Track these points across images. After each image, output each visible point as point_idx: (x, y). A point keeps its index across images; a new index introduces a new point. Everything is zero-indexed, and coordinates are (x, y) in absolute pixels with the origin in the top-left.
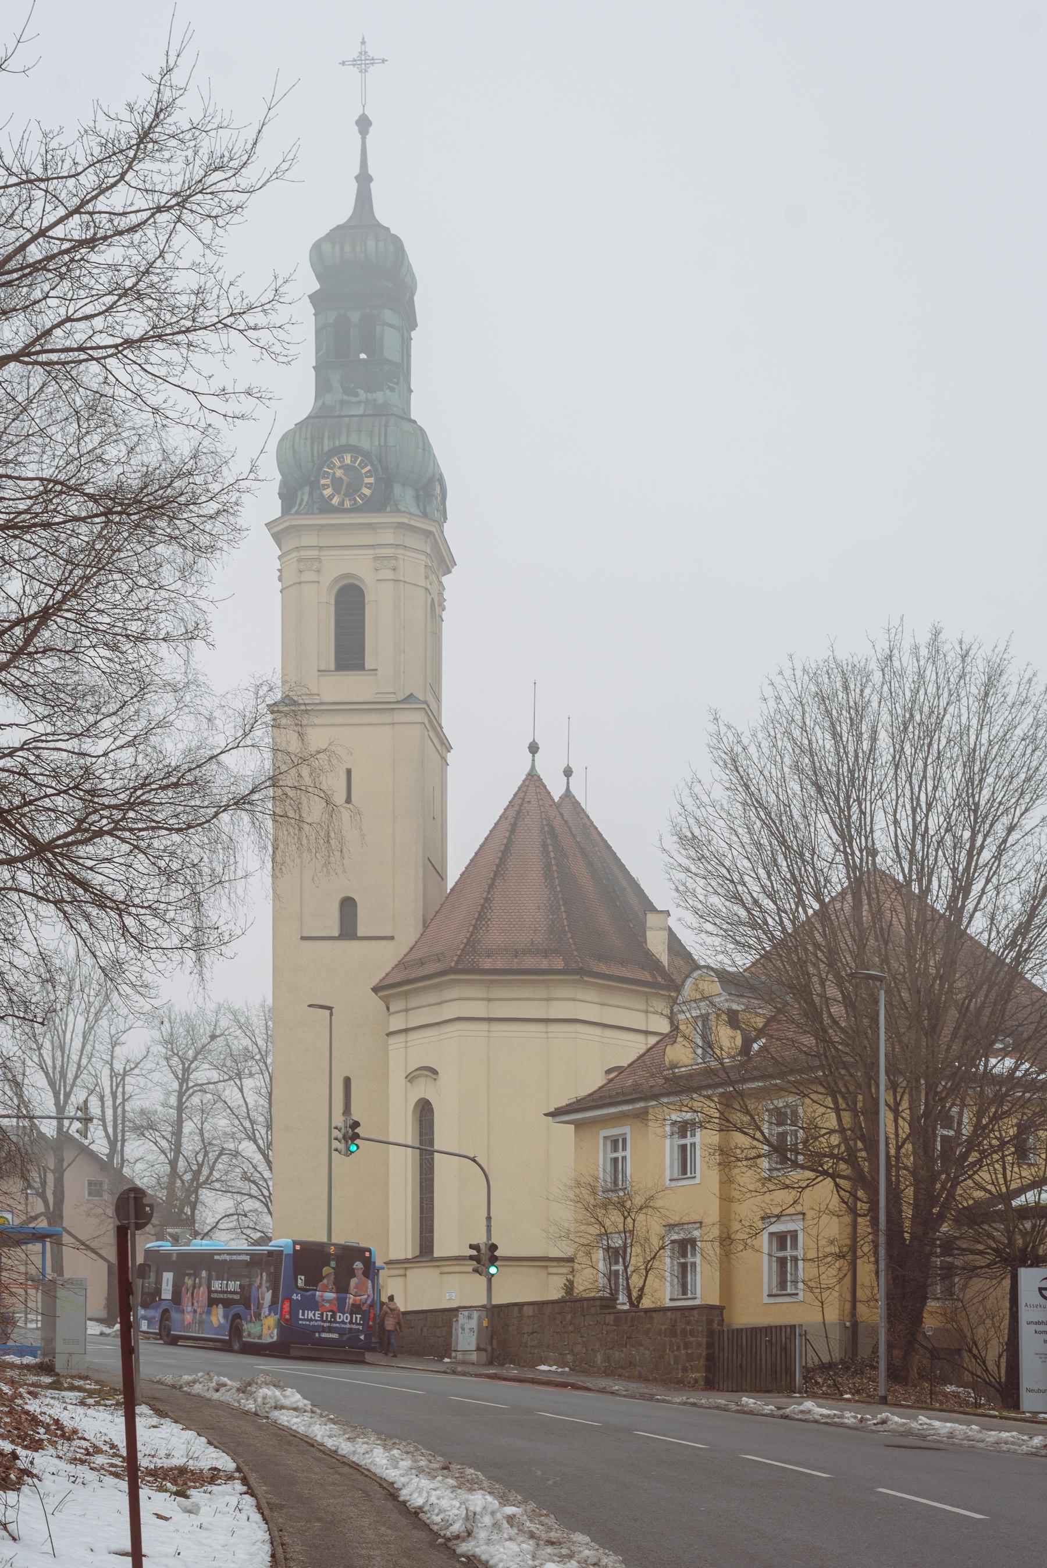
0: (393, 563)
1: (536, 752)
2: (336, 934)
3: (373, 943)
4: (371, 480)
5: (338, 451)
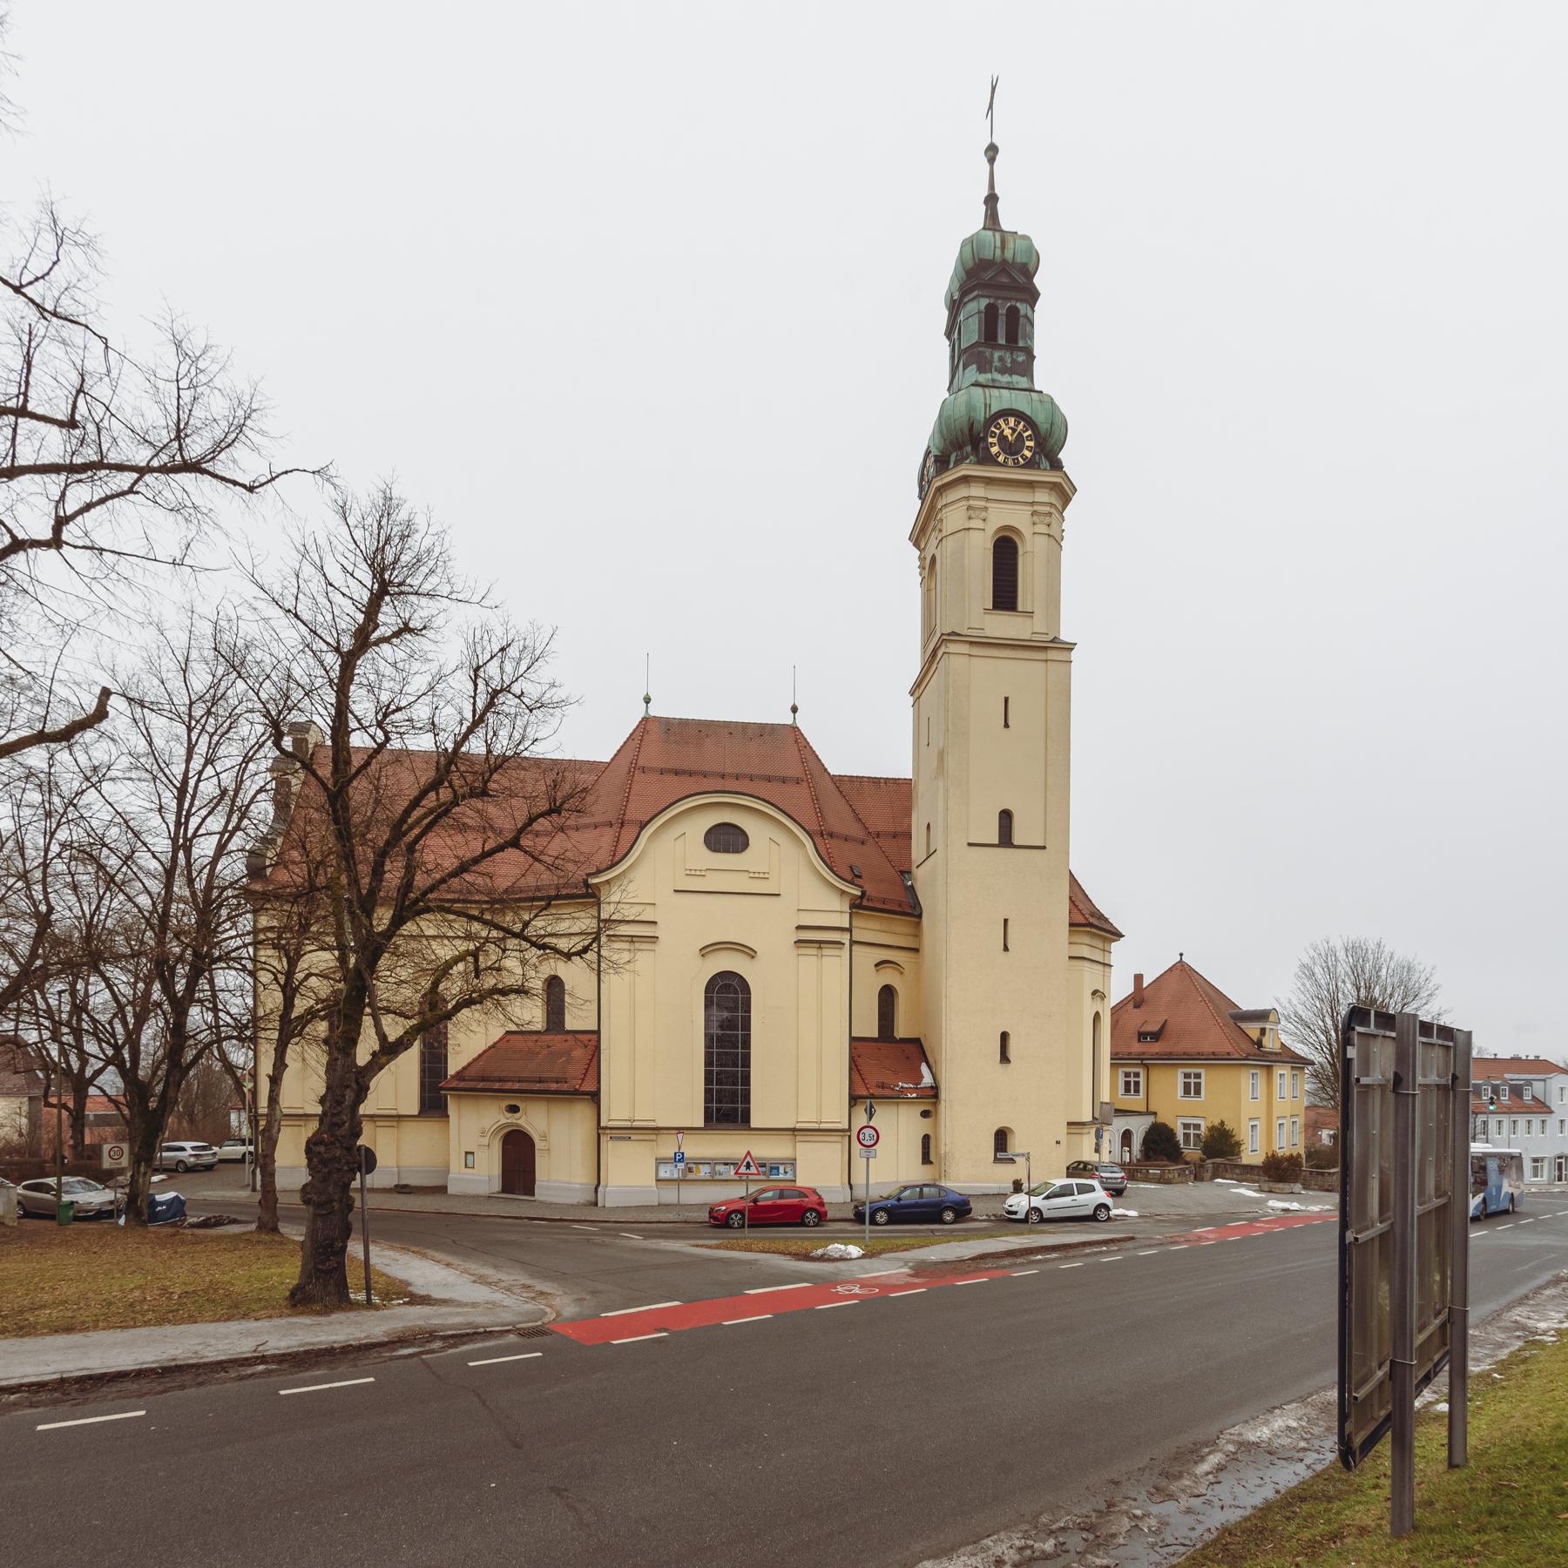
0: (1047, 520)
4: (1031, 444)
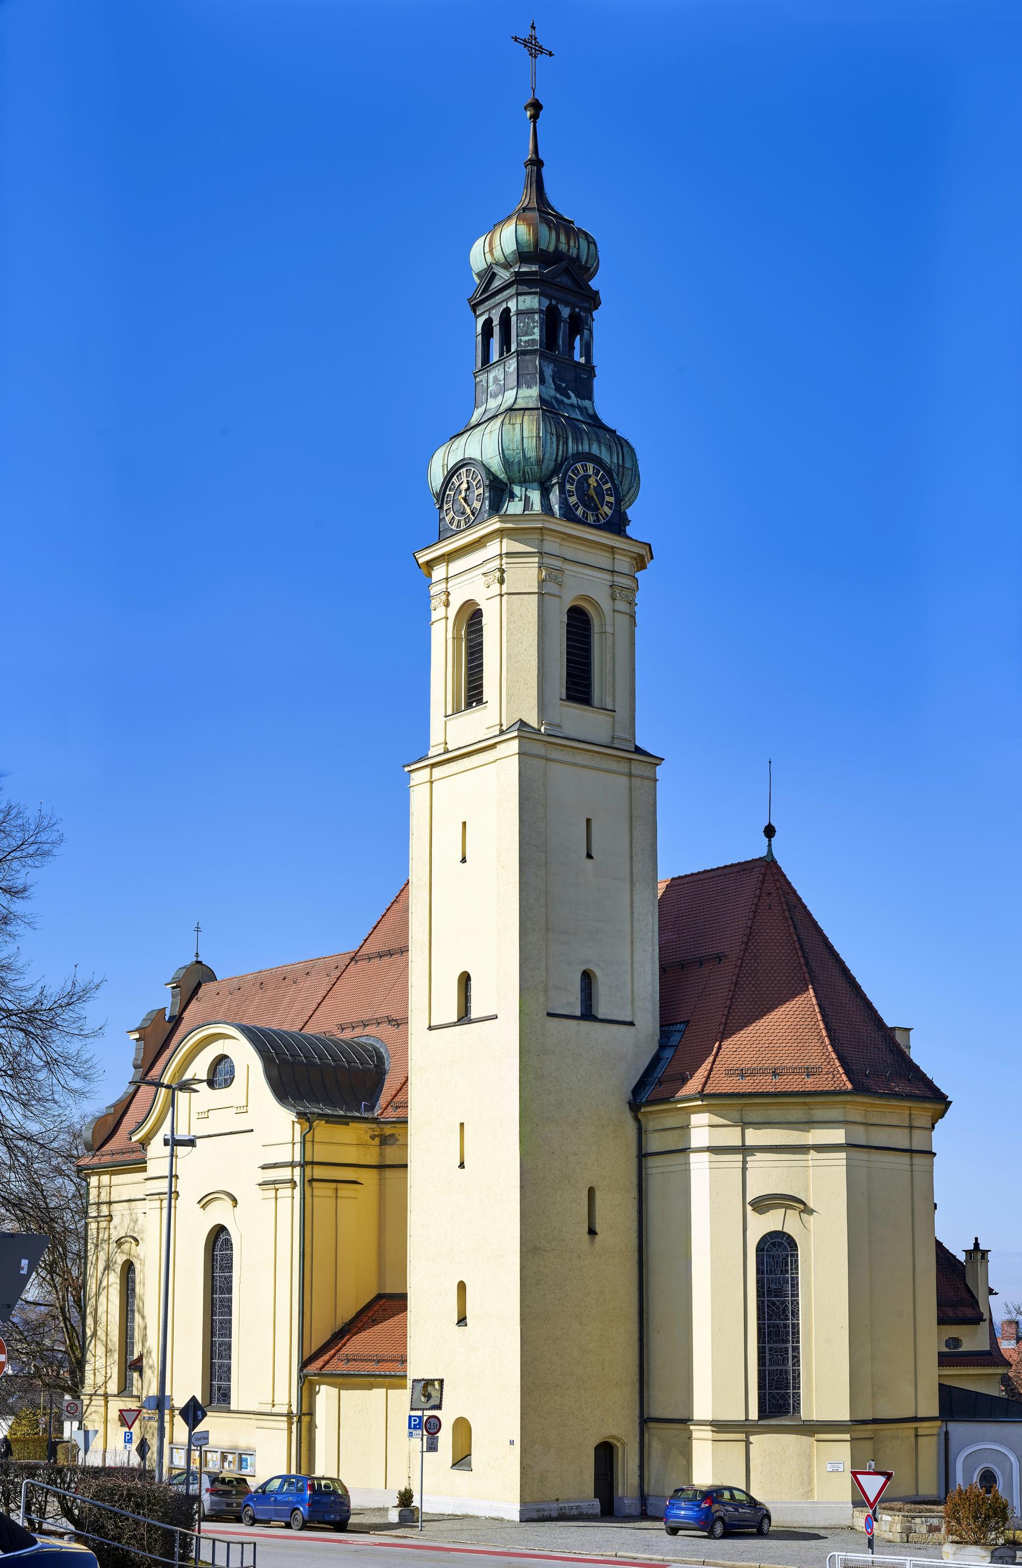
1: (766, 827)
2: (578, 1013)
3: (615, 1027)
5: (579, 457)
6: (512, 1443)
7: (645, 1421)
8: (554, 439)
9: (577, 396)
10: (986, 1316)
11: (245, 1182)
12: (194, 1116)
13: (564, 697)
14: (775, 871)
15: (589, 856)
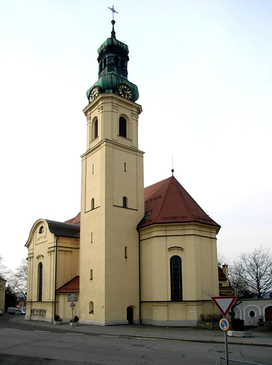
6: (103, 307)
7: (141, 302)
8: (116, 79)
9: (123, 75)
10: (228, 279)
11: (45, 253)
12: (37, 240)
13: (119, 134)
14: (175, 180)
15: (125, 171)
